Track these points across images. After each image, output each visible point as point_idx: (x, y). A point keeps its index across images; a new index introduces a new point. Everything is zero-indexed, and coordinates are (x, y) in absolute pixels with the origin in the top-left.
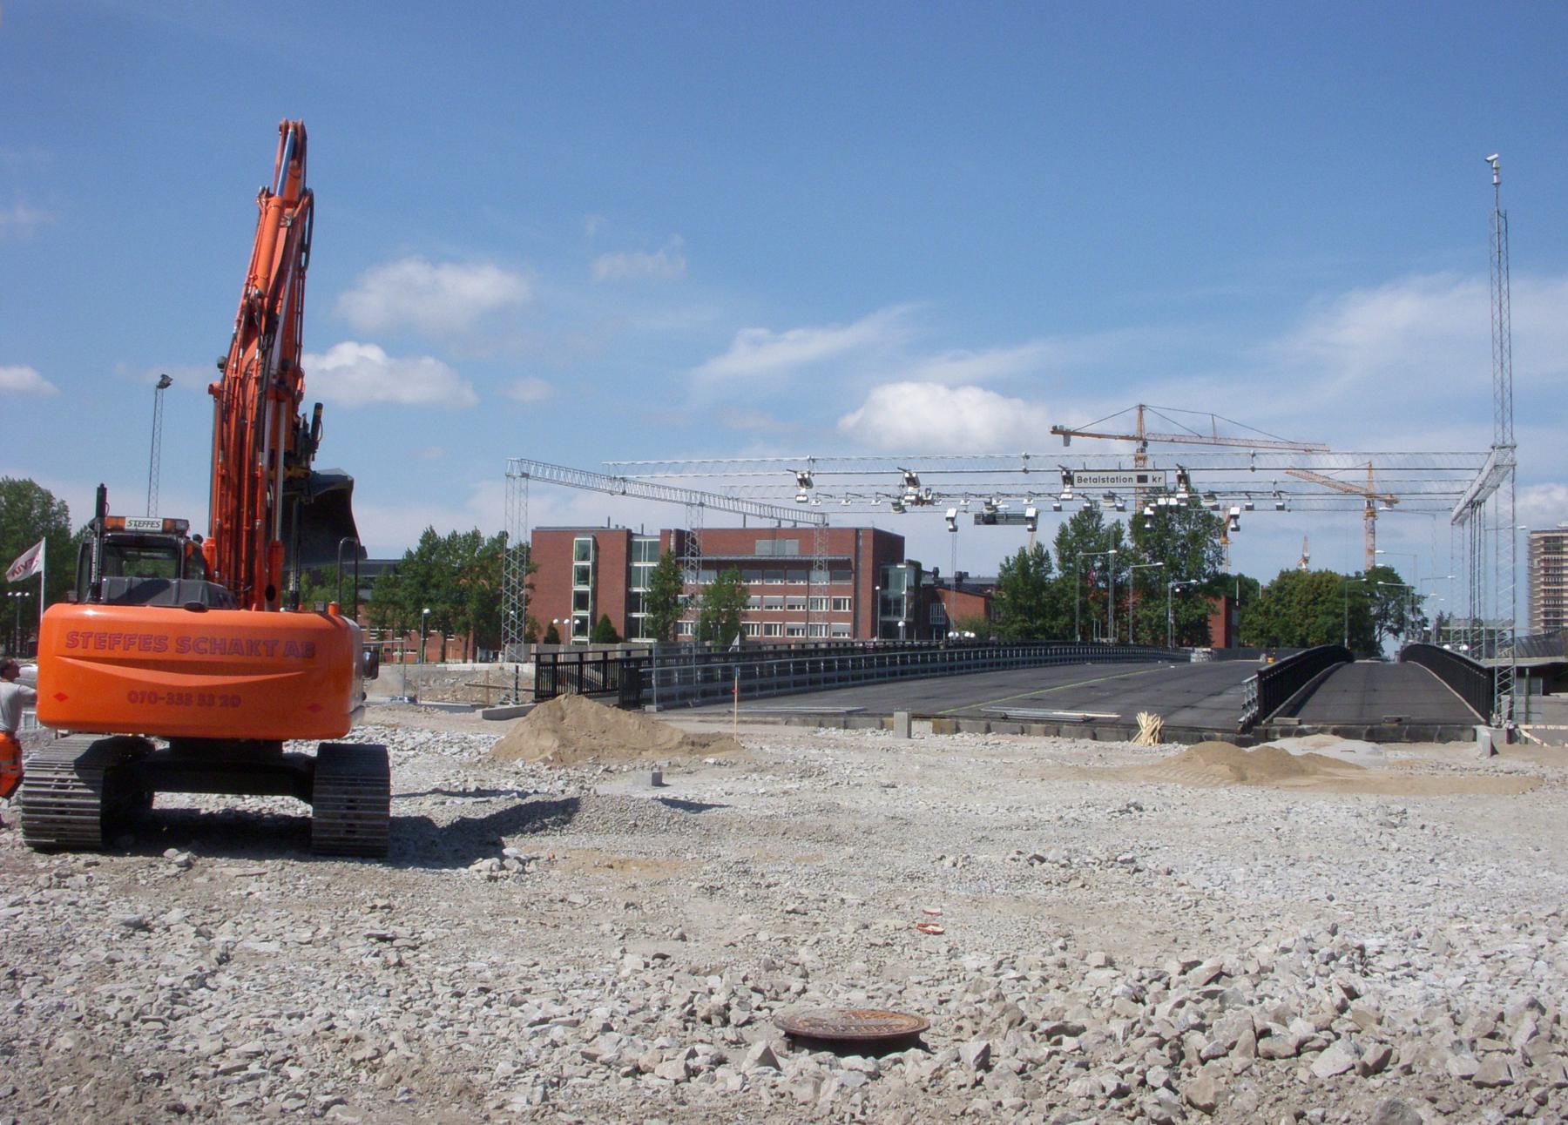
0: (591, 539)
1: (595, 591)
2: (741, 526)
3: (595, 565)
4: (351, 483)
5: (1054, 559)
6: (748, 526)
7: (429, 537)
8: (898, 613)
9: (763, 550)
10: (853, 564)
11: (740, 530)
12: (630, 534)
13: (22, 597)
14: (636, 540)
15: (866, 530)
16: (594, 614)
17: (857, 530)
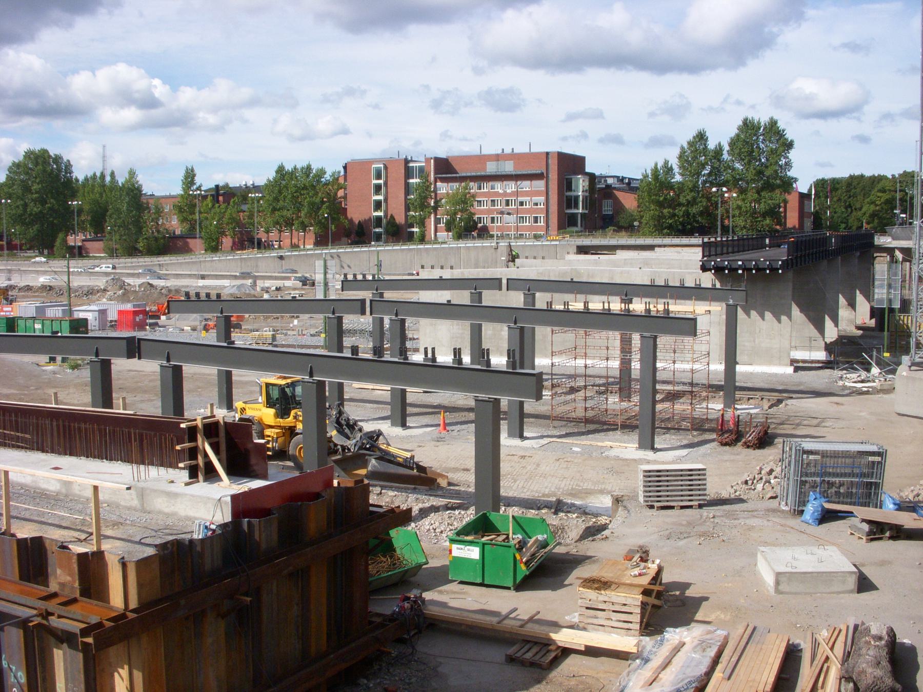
0: (382, 166)
1: (386, 200)
2: (528, 151)
3: (386, 183)
4: (227, 184)
5: (676, 169)
6: (533, 150)
7: (280, 170)
8: (576, 207)
9: (491, 168)
10: (545, 175)
11: (528, 153)
12: (407, 161)
13: (78, 204)
14: (411, 165)
15: (554, 153)
16: (386, 215)
17: (547, 154)
